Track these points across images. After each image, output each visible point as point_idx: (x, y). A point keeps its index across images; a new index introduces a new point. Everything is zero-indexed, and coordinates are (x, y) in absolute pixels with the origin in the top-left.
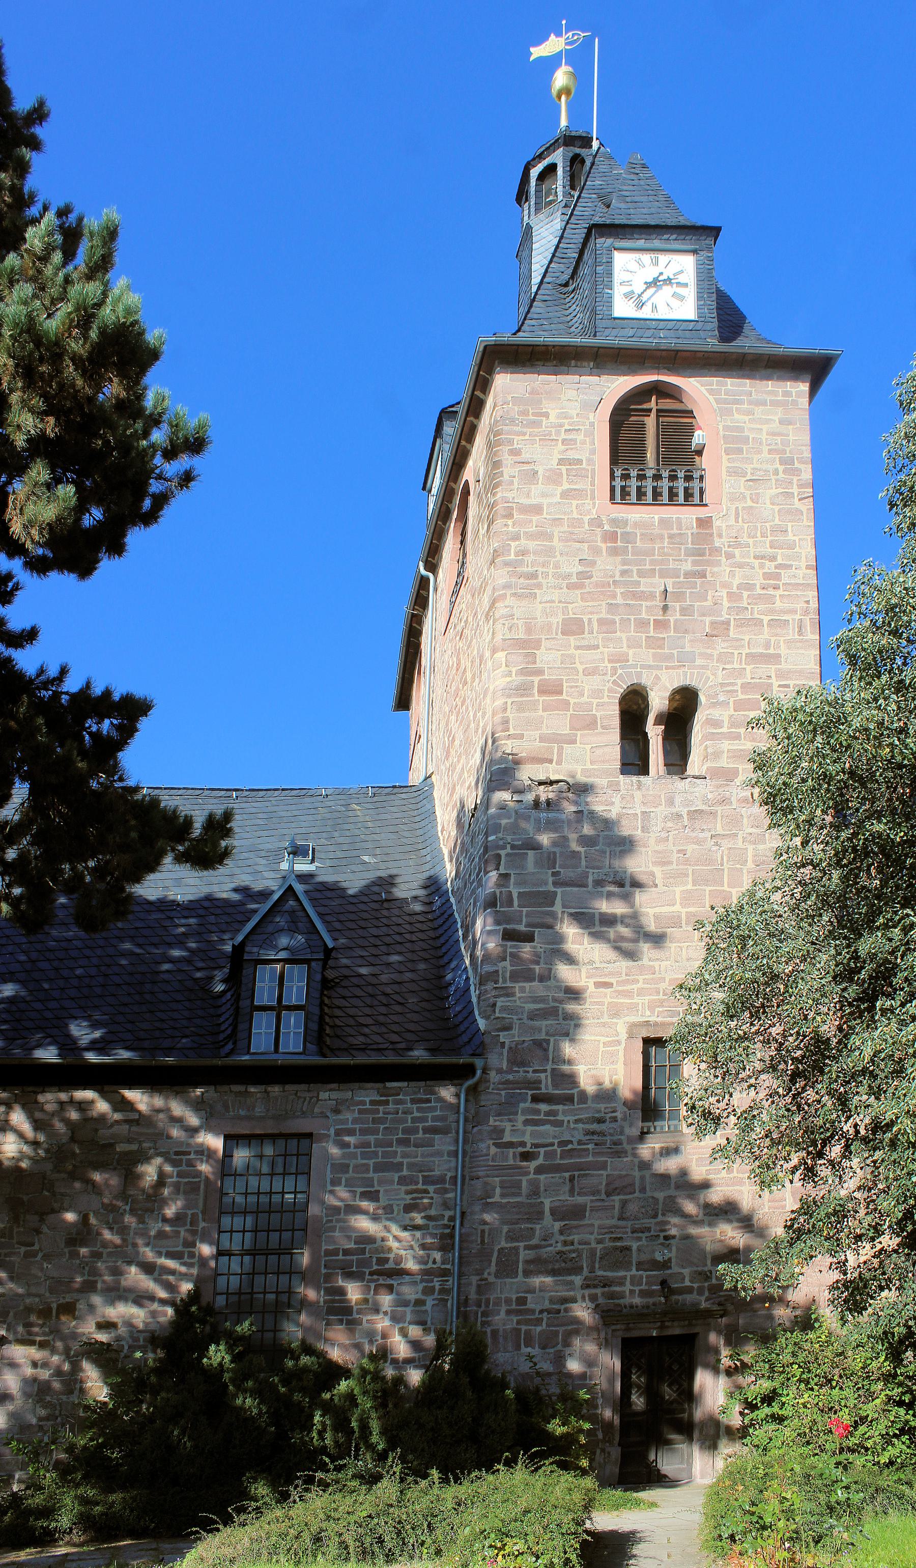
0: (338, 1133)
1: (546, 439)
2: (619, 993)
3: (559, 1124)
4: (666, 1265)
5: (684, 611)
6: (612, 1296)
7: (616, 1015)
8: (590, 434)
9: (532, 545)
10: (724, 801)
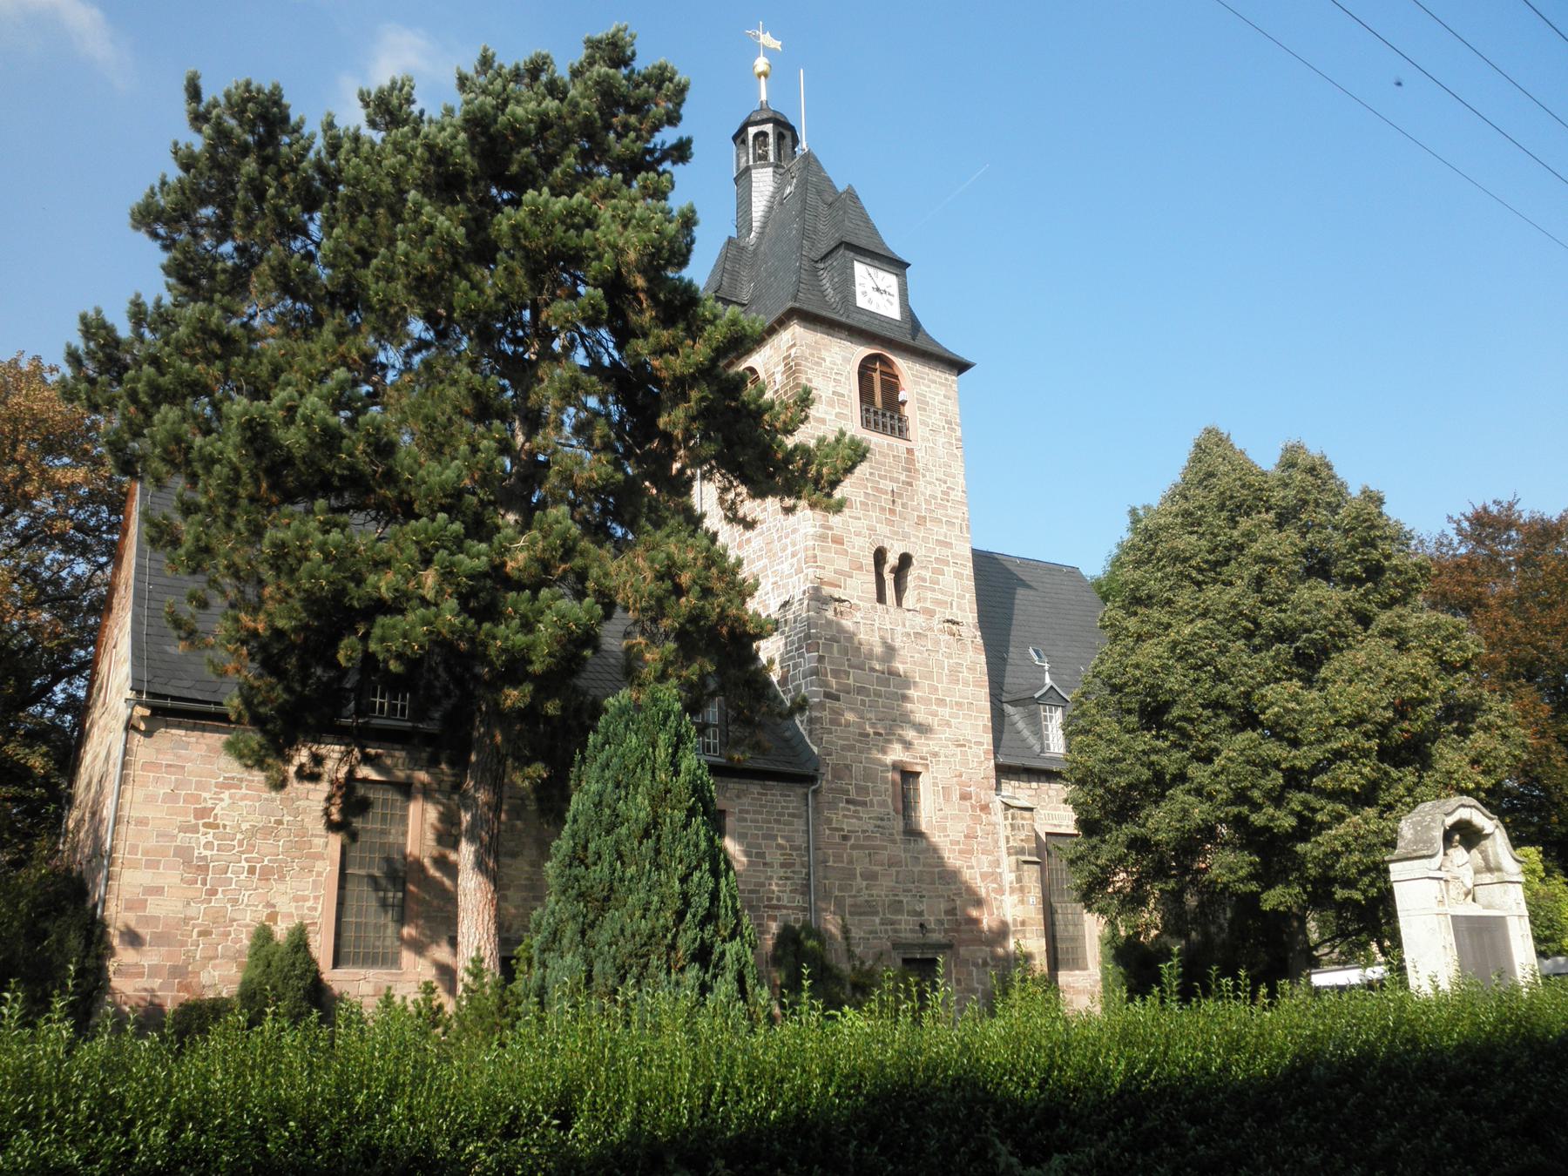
0: (741, 811)
3: (860, 819)
5: (904, 505)
6: (895, 931)
8: (848, 378)
10: (931, 629)
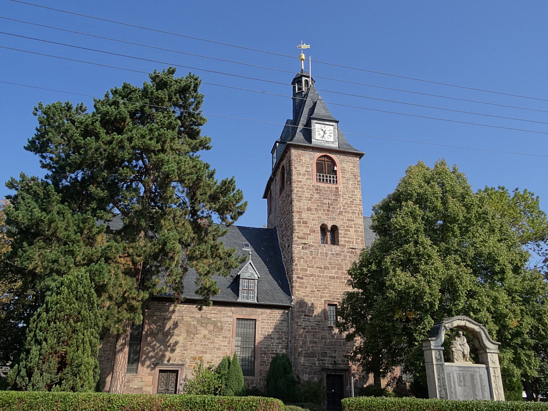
1: (302, 166)
2: (322, 293)
4: (335, 357)
5: (333, 208)
6: (324, 364)
7: (321, 298)
8: (311, 165)
9: (300, 190)
